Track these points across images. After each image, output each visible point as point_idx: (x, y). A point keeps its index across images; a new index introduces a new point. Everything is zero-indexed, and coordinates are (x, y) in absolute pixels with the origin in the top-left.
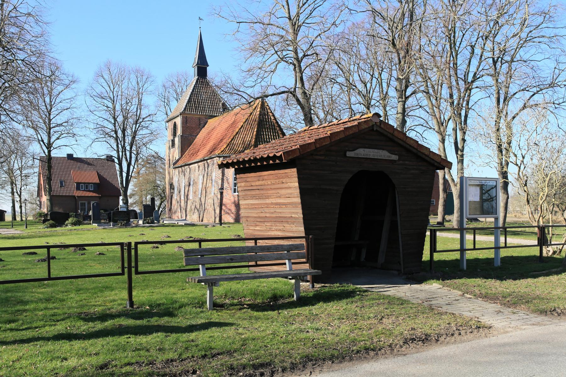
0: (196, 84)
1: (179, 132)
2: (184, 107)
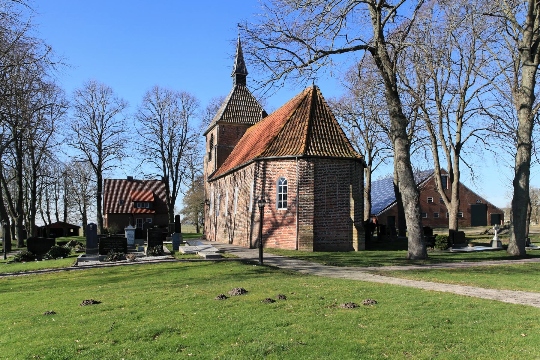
1: (216, 143)
2: (221, 115)
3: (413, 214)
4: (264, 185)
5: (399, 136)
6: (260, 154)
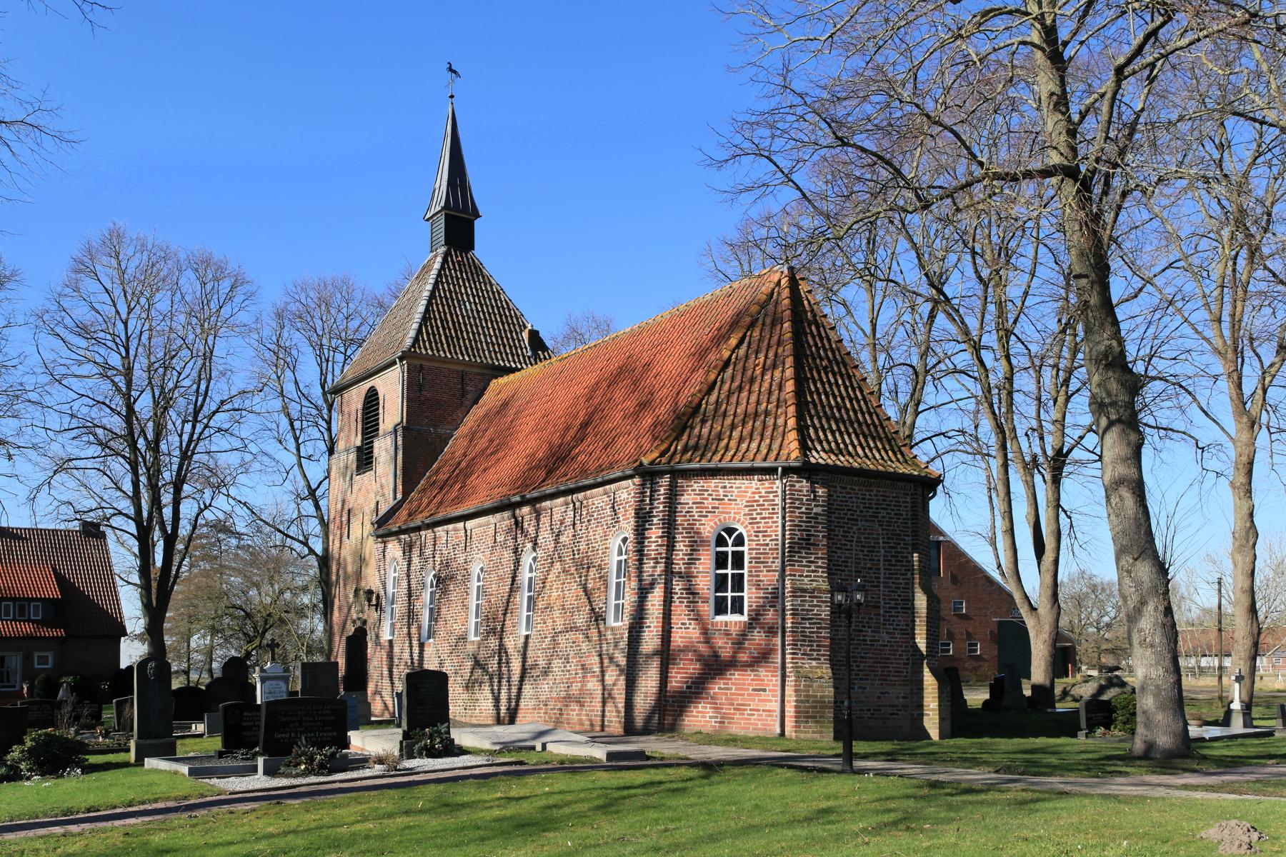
0: (442, 267)
3: (1159, 633)
4: (671, 546)
5: (1119, 421)
6: (656, 454)
